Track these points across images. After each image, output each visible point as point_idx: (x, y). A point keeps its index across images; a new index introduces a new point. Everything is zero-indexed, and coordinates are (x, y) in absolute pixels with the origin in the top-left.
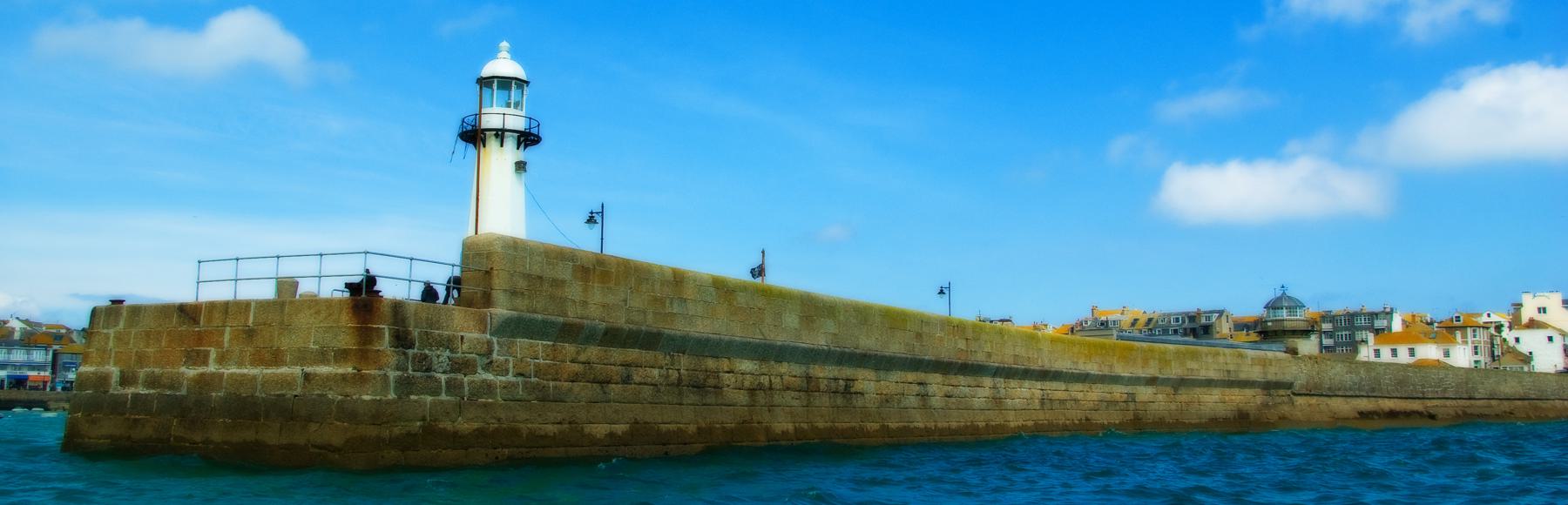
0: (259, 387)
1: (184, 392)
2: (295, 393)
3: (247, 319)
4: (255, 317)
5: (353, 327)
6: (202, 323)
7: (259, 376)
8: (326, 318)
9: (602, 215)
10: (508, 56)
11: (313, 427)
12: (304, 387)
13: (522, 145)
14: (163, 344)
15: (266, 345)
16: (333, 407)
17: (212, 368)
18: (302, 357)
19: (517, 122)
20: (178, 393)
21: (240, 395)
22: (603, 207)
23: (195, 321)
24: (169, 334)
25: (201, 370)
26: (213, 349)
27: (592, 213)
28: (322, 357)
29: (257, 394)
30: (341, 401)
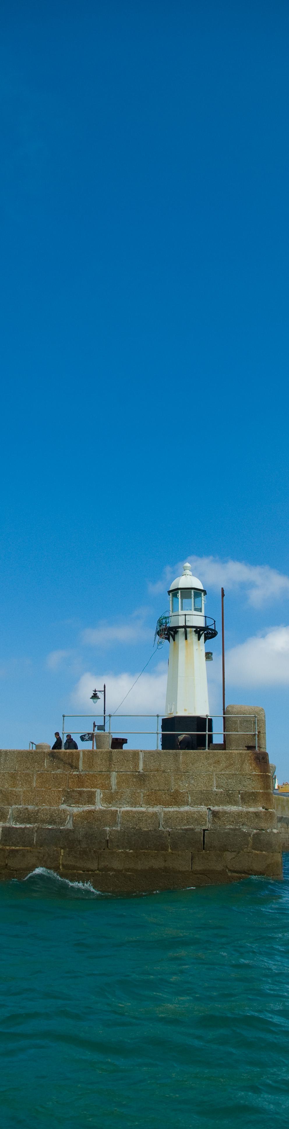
0: (162, 822)
1: (69, 826)
2: (204, 828)
3: (137, 765)
4: (144, 761)
5: (258, 775)
6: (81, 766)
7: (160, 814)
8: (227, 767)
9: (105, 693)
10: (191, 573)
11: (229, 856)
12: (214, 823)
13: (202, 638)
14: (34, 784)
15: (162, 788)
16: (250, 839)
17: (99, 806)
18: (205, 798)
19: (199, 621)
20: (62, 828)
21: (140, 829)
22: (105, 687)
23: (74, 767)
24: (40, 776)
25: (87, 808)
26: (98, 791)
27: (95, 691)
28: (229, 798)
29: (161, 828)
30: (256, 834)
